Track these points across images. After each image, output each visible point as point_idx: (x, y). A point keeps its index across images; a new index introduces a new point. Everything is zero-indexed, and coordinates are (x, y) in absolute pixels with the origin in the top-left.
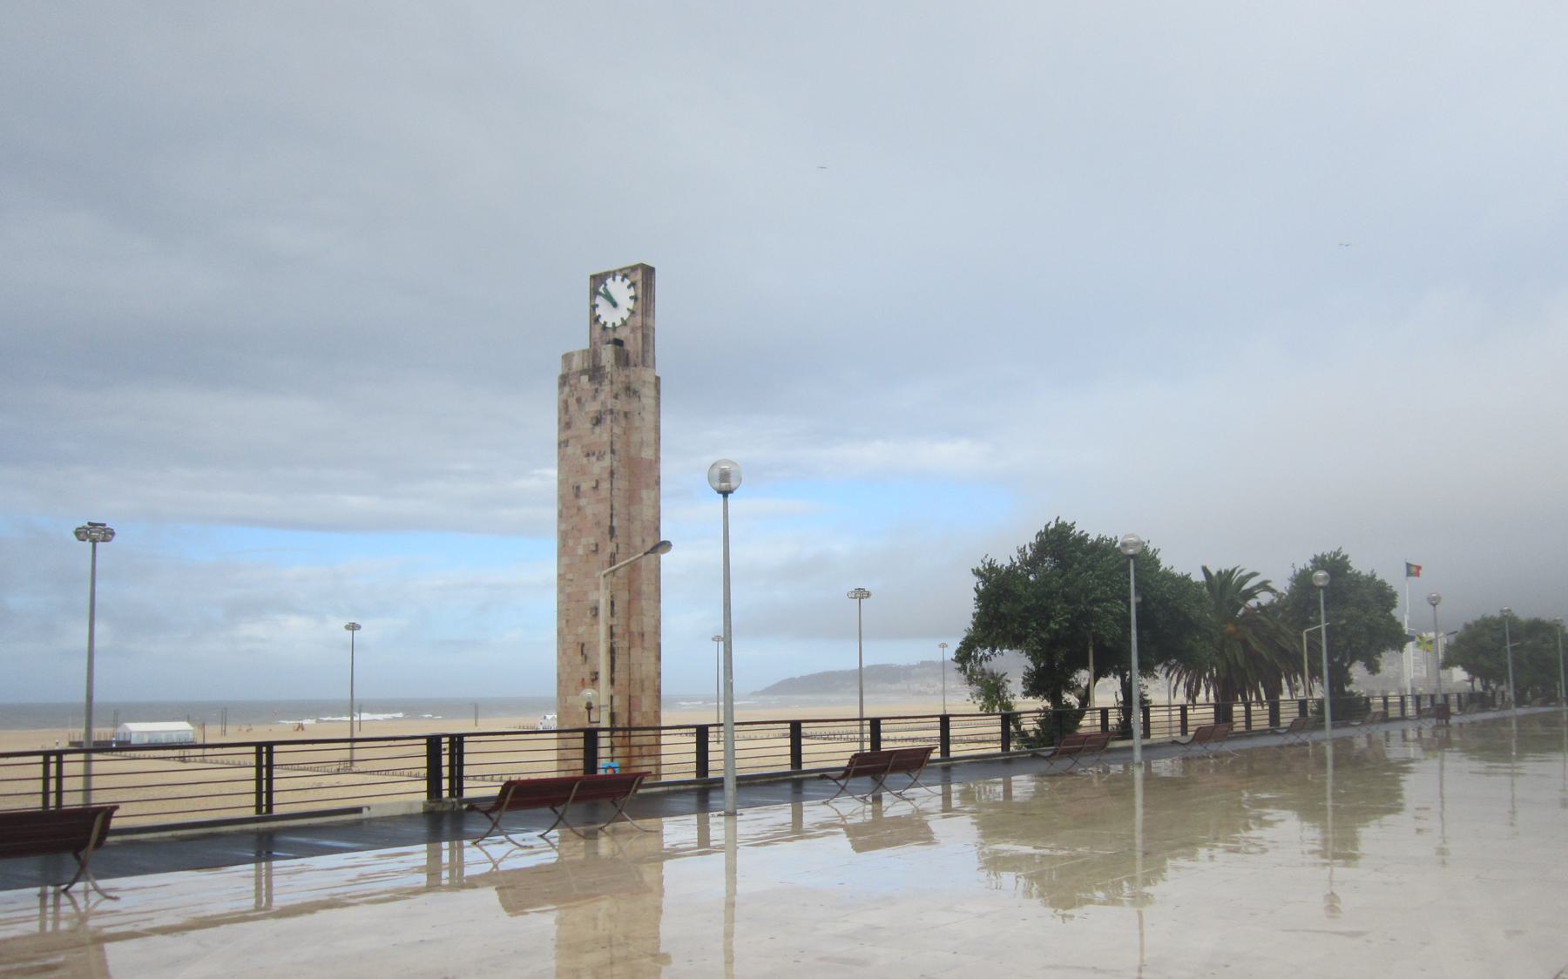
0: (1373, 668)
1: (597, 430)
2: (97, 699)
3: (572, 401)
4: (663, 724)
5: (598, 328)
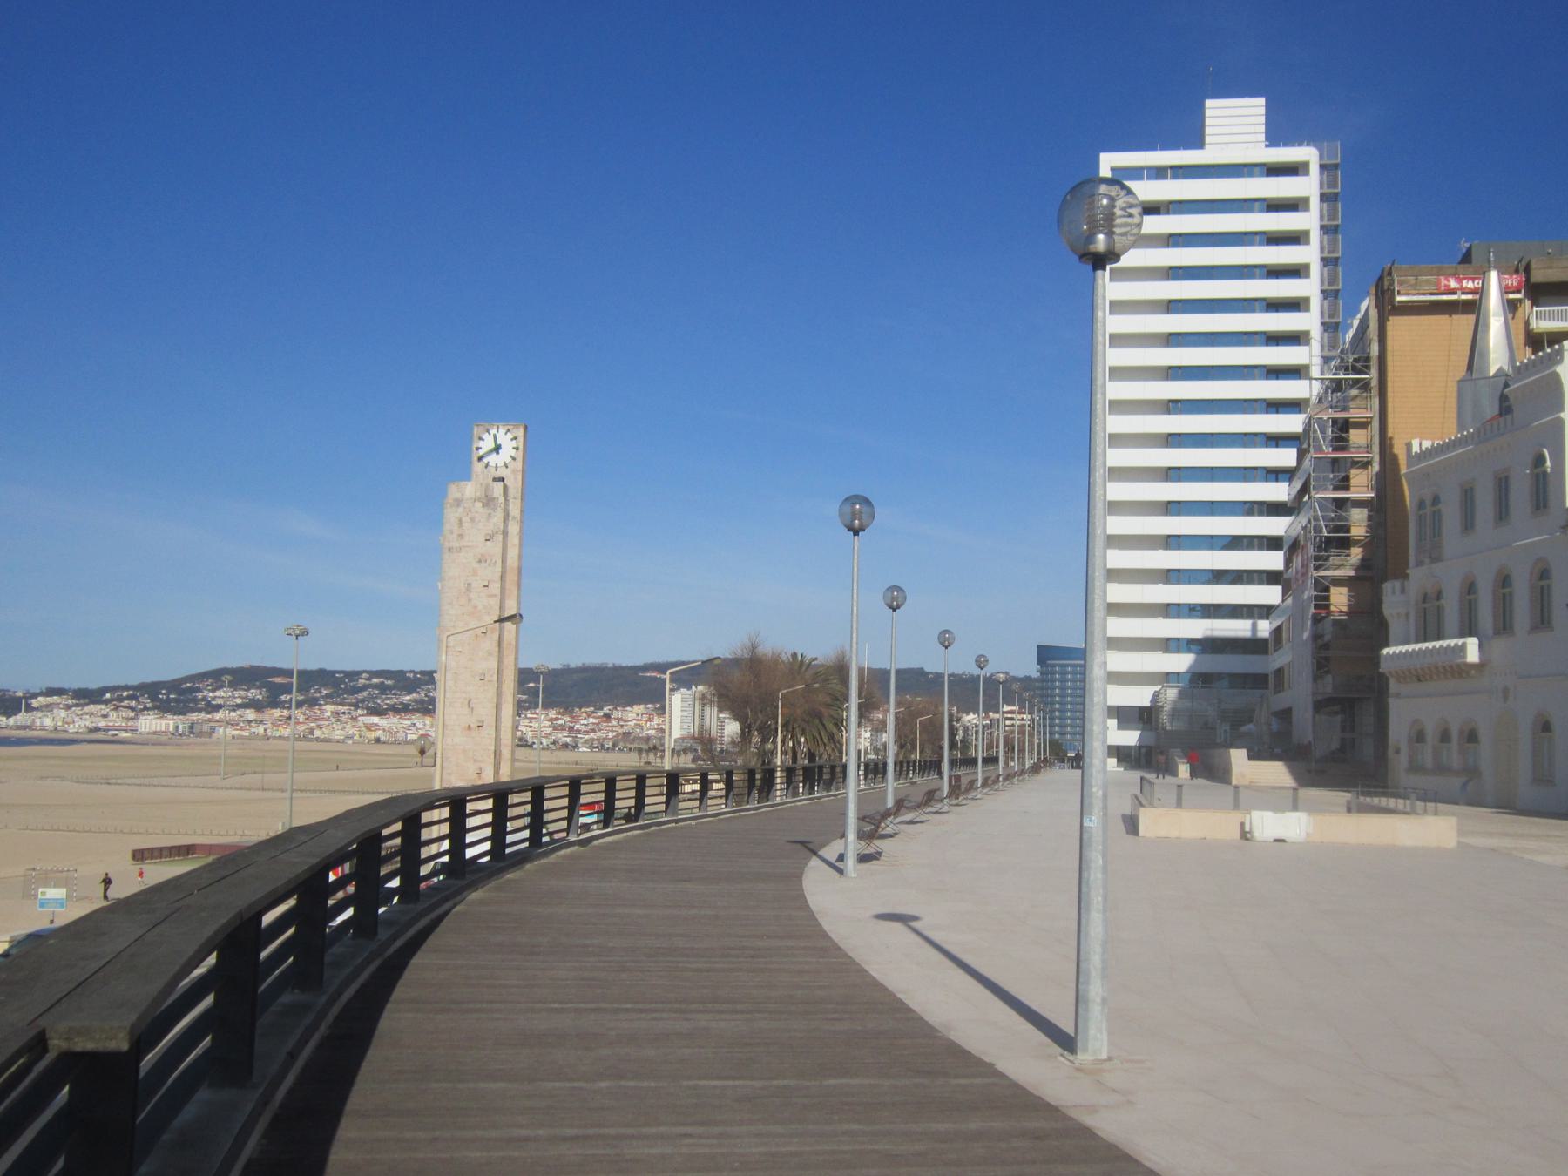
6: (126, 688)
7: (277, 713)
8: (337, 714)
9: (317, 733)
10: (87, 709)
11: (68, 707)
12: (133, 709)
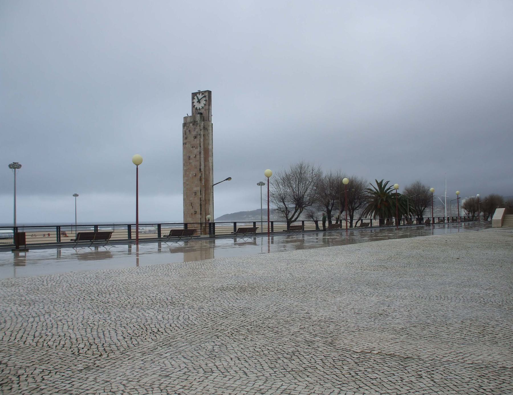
1: (195, 140)
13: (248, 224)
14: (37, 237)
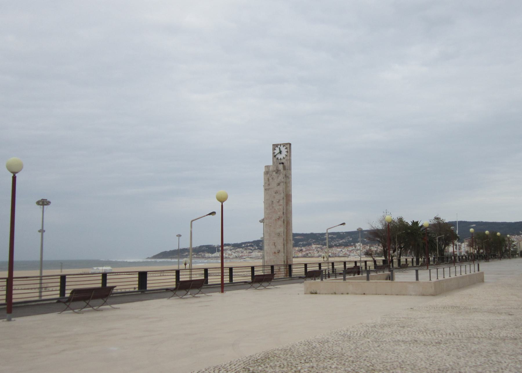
0: (513, 242)
1: (279, 187)
2: (44, 259)
3: (270, 178)
4: (193, 268)
5: (275, 159)
6: (249, 242)
7: (297, 249)
8: (316, 248)
9: (310, 255)
10: (236, 250)
11: (231, 250)
12: (251, 250)
13: (17, 288)
14: (51, 289)
